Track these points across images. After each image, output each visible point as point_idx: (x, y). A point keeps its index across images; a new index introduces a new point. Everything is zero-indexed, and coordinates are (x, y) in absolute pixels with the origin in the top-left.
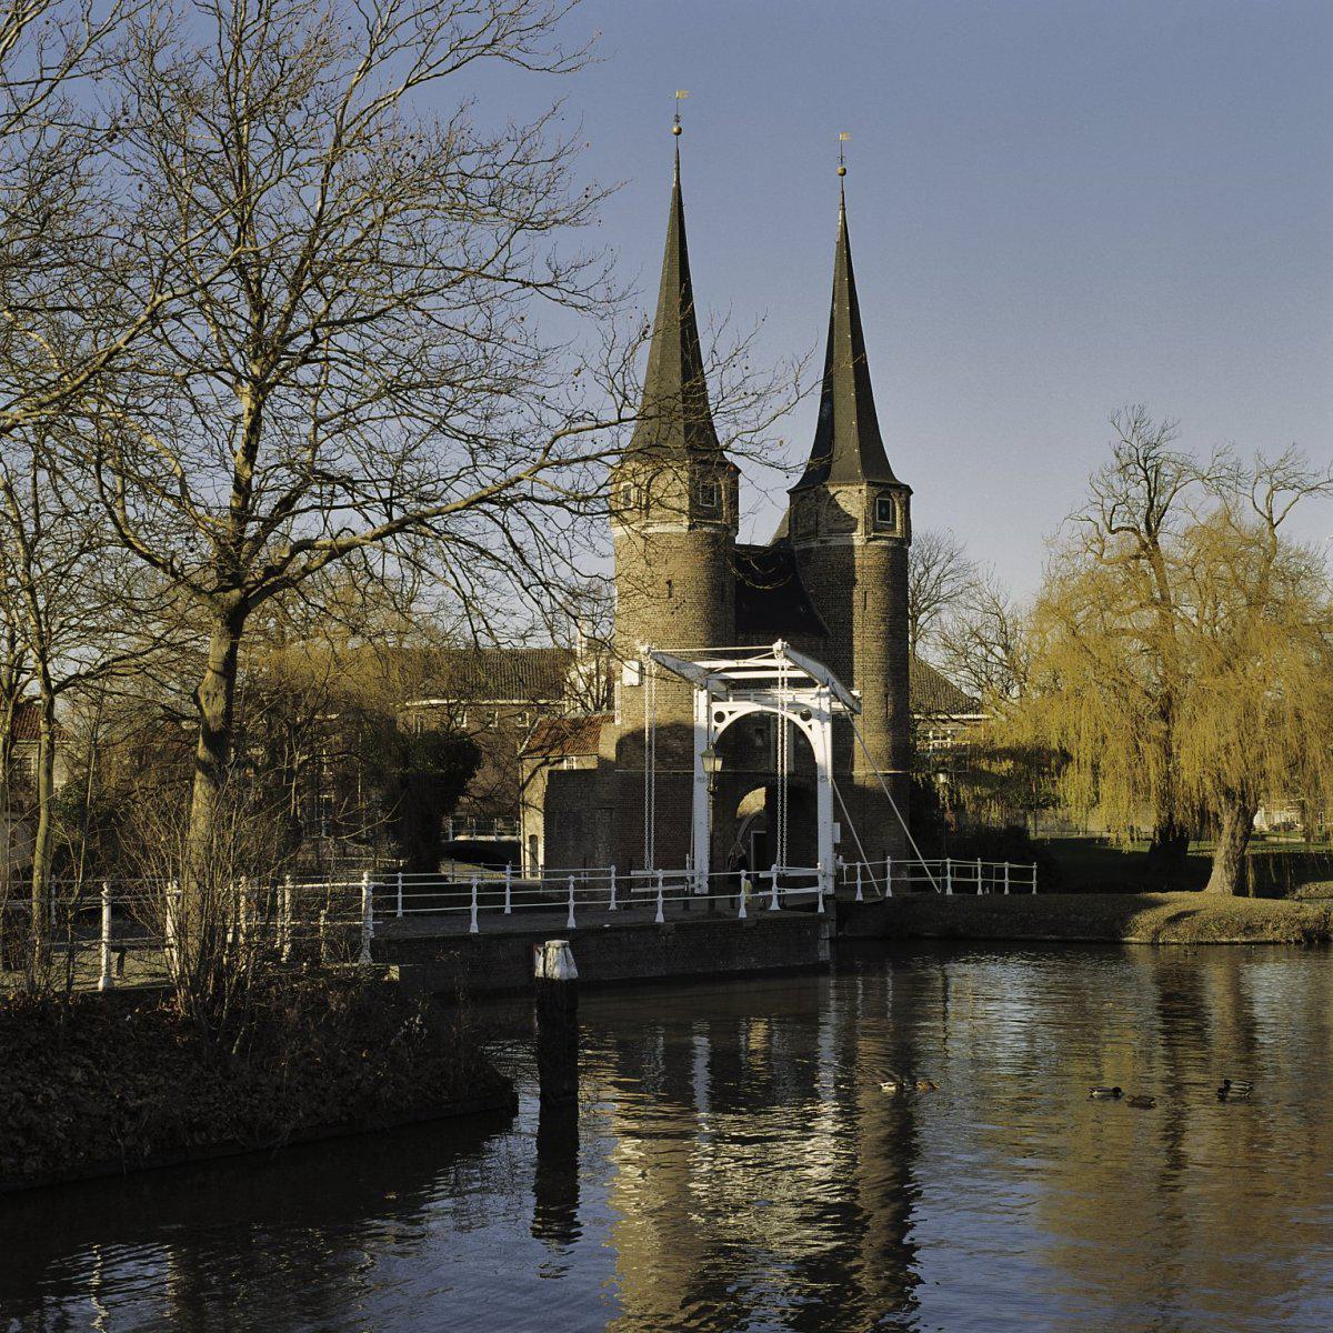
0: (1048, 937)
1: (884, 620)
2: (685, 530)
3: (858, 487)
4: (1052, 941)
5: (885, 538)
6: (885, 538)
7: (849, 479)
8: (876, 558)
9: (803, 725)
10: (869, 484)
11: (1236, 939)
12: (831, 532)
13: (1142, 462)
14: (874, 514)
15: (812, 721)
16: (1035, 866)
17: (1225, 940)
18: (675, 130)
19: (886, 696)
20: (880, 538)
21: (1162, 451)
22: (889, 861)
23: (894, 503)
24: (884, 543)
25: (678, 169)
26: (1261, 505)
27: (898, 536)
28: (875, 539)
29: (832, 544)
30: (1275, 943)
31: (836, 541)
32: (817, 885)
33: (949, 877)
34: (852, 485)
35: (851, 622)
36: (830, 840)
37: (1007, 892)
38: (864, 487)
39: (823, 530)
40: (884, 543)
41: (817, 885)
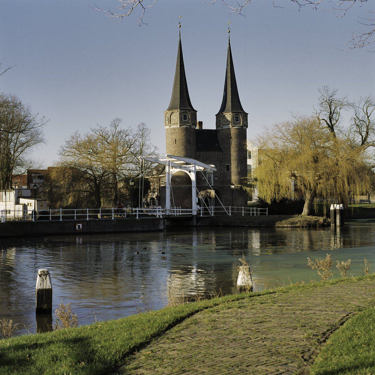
0: (246, 225)
1: (237, 147)
2: (179, 127)
3: (229, 114)
4: (247, 226)
5: (237, 126)
6: (237, 126)
7: (228, 112)
8: (234, 131)
9: (189, 174)
10: (232, 112)
11: (288, 226)
12: (223, 125)
13: (328, 101)
14: (234, 120)
15: (191, 173)
16: (267, 209)
17: (286, 226)
18: (179, 26)
19: (238, 166)
20: (236, 126)
21: (335, 97)
22: (243, 207)
23: (240, 117)
24: (237, 127)
25: (180, 36)
26: (365, 110)
27: (241, 125)
28: (234, 126)
29: (224, 128)
30: (299, 227)
31: (225, 127)
32: (192, 212)
33: (243, 212)
34: (228, 113)
35: (230, 149)
36: (195, 202)
37: (251, 215)
38: (231, 113)
39: (221, 125)
40: (237, 127)
41: (192, 212)
